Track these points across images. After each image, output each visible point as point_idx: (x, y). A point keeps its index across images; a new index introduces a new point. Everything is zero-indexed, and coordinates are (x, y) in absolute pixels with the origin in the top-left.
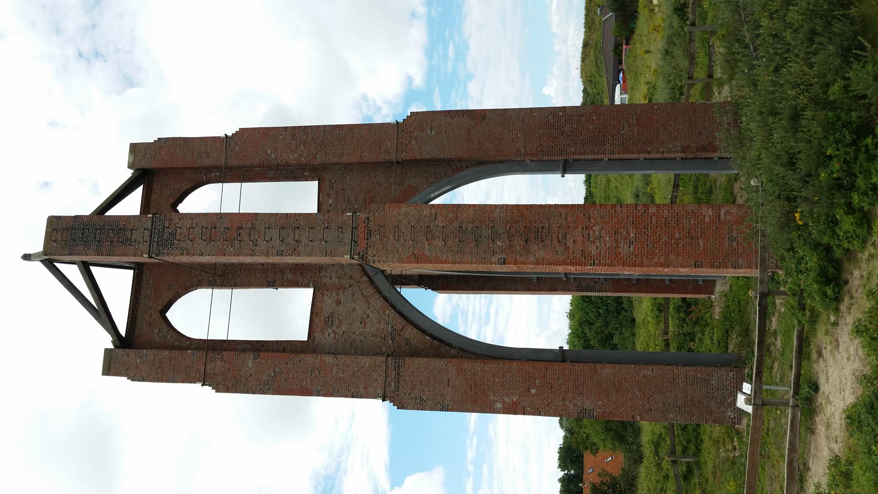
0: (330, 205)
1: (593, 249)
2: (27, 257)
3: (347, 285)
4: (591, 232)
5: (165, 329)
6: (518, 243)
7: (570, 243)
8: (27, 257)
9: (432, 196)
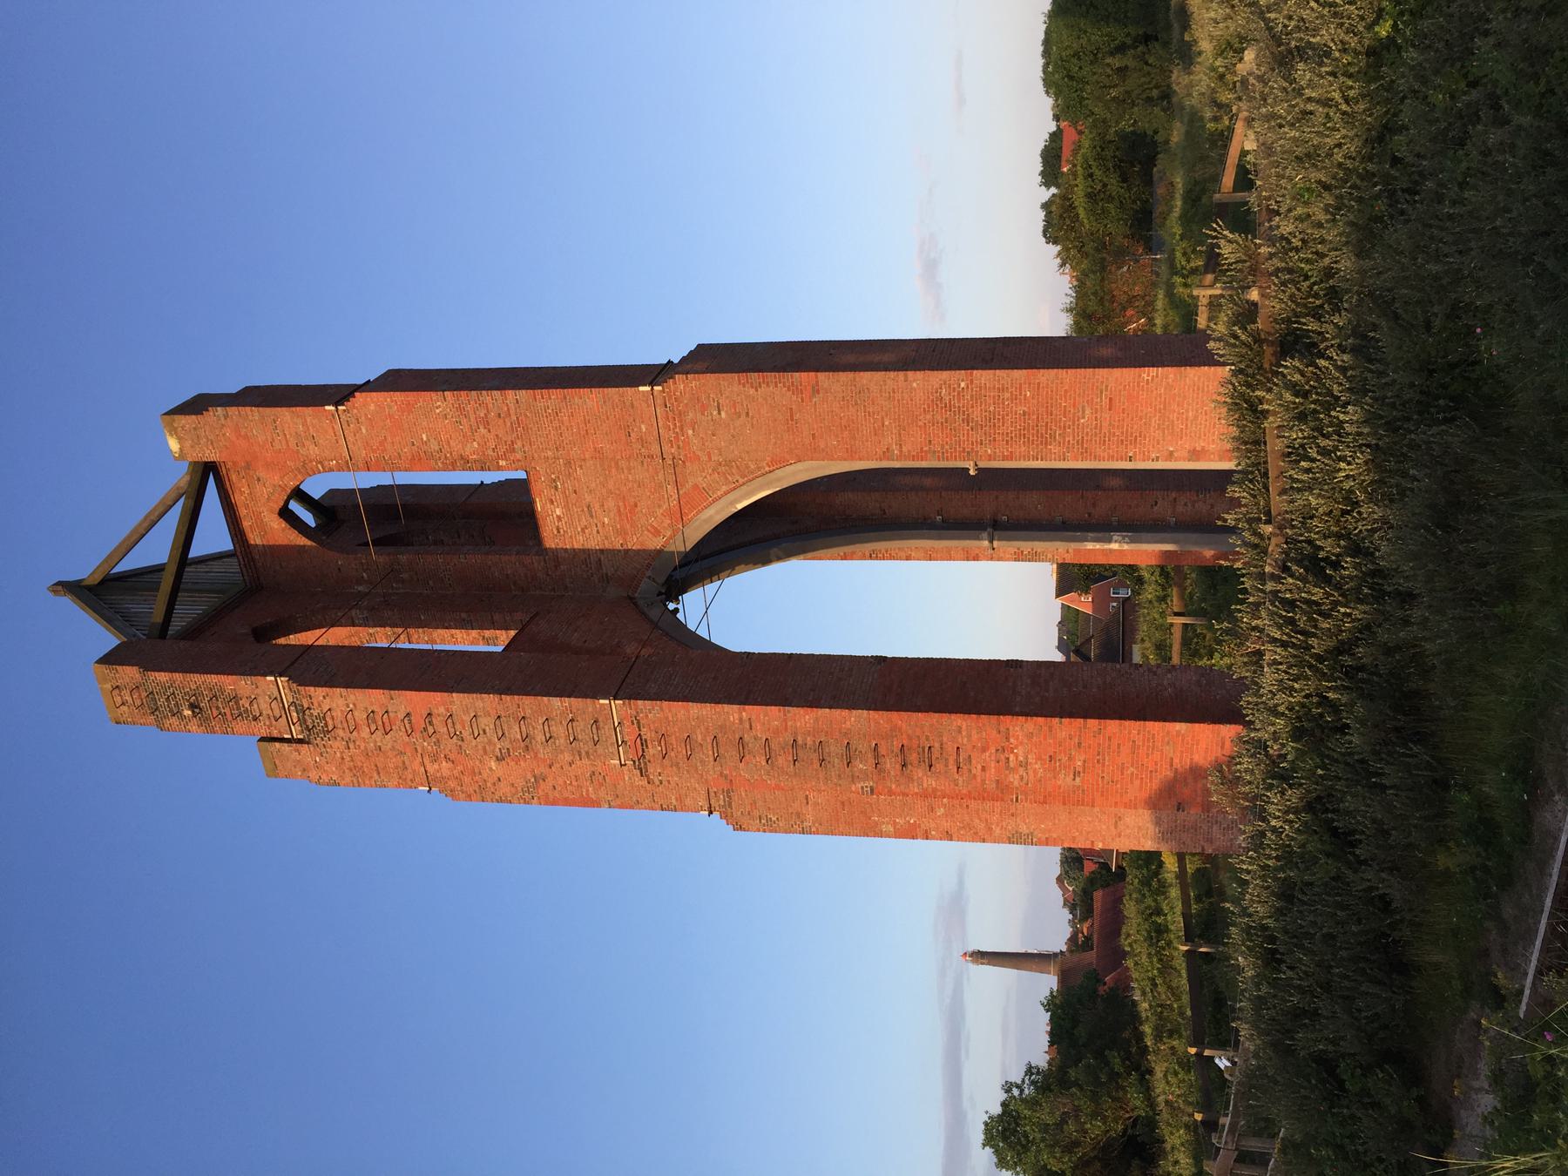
0: (559, 518)
1: (1014, 779)
4: (1012, 757)
7: (977, 770)
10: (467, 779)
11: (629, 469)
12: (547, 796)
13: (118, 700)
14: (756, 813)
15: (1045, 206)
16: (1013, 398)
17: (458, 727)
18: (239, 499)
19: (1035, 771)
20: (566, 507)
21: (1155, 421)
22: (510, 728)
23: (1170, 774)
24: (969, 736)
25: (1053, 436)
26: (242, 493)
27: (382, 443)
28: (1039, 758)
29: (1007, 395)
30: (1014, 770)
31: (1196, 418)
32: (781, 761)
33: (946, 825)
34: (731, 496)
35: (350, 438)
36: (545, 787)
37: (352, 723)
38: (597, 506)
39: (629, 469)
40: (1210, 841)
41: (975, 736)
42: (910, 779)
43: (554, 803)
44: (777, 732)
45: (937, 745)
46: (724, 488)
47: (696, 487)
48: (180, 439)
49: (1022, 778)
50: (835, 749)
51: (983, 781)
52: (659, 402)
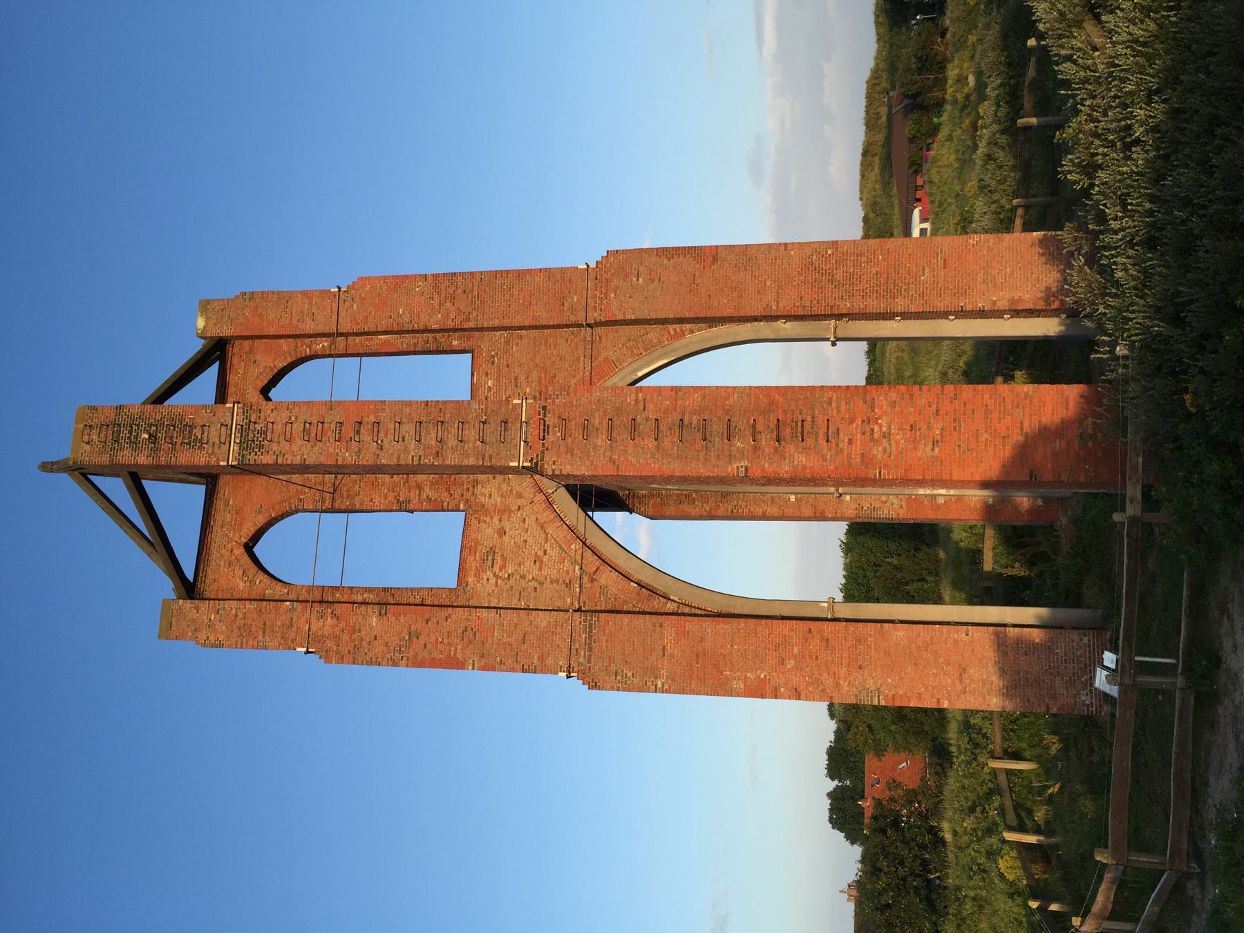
0: (490, 388)
1: (877, 452)
2: (48, 467)
3: (514, 508)
4: (876, 428)
5: (253, 569)
6: (766, 440)
7: (844, 445)
8: (48, 467)
9: (640, 374)
10: (345, 637)
11: (556, 345)
12: (416, 656)
13: (86, 439)
14: (613, 668)
15: (830, 795)
16: (869, 261)
17: (382, 435)
18: (232, 379)
19: (897, 443)
20: (498, 380)
21: (980, 278)
22: (428, 433)
23: (1021, 438)
24: (838, 407)
25: (899, 291)
26: (237, 373)
27: (366, 318)
28: (901, 429)
29: (864, 259)
30: (877, 442)
31: (1012, 273)
32: (666, 442)
33: (795, 680)
34: (633, 366)
35: (342, 314)
36: (417, 645)
37: (288, 434)
38: (523, 378)
39: (556, 345)
40: (1054, 697)
41: (843, 408)
42: (783, 457)
43: (421, 665)
44: (667, 412)
45: (809, 418)
46: (630, 360)
47: (606, 360)
48: (208, 319)
49: (885, 450)
50: (717, 428)
51: (849, 455)
52: (591, 277)
